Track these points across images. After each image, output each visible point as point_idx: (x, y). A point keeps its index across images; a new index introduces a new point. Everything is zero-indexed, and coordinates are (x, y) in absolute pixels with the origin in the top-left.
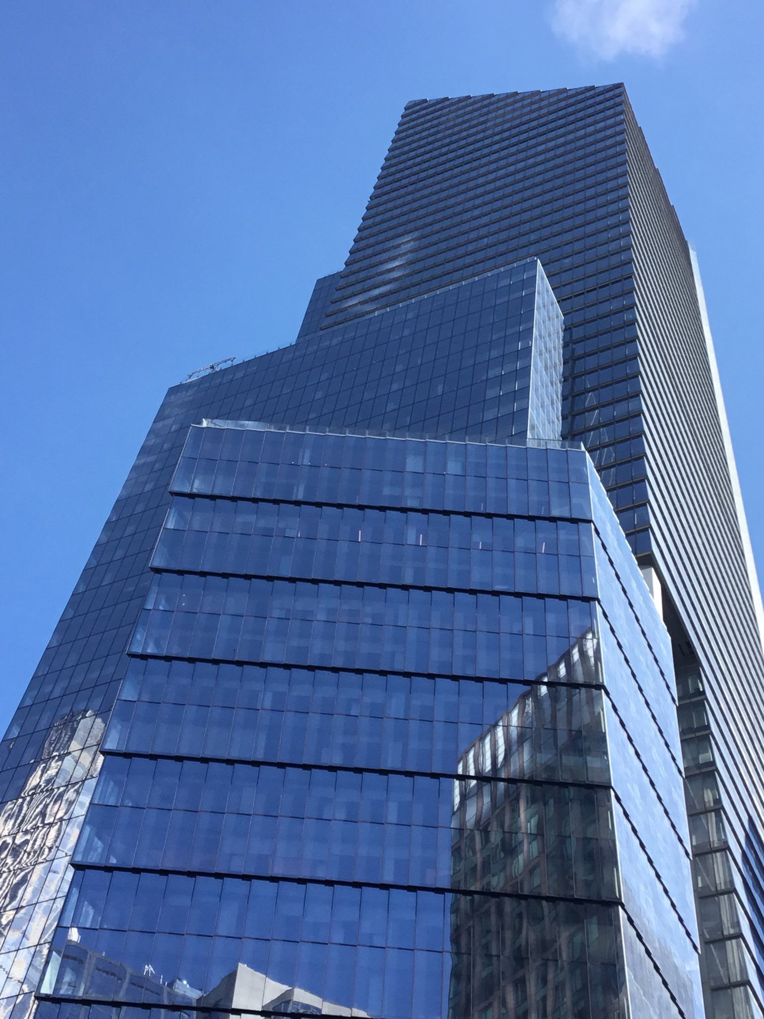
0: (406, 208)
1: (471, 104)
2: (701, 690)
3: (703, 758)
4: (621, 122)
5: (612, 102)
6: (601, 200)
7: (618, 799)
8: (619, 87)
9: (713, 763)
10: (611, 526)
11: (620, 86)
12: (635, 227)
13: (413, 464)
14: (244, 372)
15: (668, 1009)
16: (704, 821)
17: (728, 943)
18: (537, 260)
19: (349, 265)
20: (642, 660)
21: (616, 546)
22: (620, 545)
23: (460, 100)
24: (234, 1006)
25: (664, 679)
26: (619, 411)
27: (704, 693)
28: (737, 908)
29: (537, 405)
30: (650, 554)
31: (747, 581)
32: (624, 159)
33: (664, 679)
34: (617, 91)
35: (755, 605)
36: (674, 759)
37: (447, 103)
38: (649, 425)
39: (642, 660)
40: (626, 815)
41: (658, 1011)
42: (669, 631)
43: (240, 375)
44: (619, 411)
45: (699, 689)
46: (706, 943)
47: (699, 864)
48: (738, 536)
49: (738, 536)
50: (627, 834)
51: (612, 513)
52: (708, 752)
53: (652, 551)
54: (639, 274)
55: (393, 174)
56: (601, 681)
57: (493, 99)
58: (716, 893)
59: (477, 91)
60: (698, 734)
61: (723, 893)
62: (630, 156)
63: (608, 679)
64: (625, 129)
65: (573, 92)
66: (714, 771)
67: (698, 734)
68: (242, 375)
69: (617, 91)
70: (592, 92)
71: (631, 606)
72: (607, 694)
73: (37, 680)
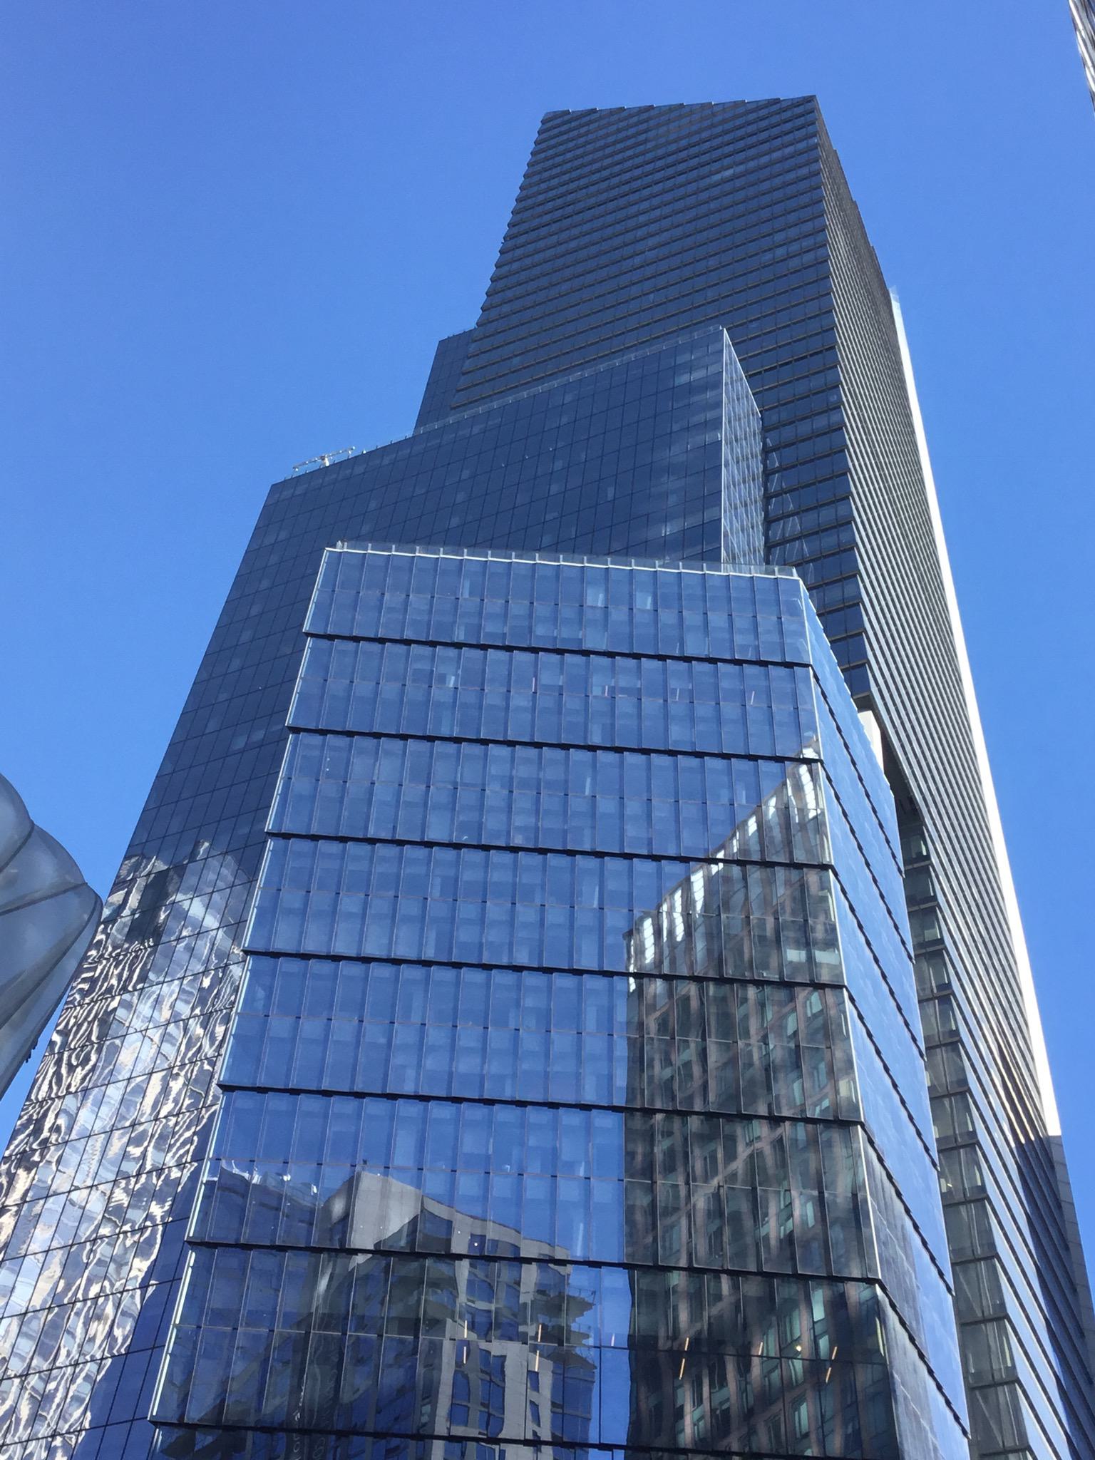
0: (566, 177)
1: (626, 119)
2: (925, 853)
3: (929, 935)
4: (815, 147)
5: (803, 132)
6: (790, 190)
7: (852, 999)
8: (810, 101)
9: (941, 941)
10: (830, 667)
11: (811, 99)
12: (837, 301)
13: (595, 598)
14: (365, 466)
15: (857, 785)
16: (984, 1327)
17: (1000, 1389)
18: (723, 330)
19: (491, 295)
20: (867, 826)
21: (836, 692)
22: (840, 690)
23: (612, 112)
24: (436, 1433)
25: (890, 847)
26: (827, 515)
27: (935, 898)
28: (992, 1224)
29: (737, 529)
30: (868, 696)
31: (1008, 938)
32: (817, 168)
33: (890, 847)
34: (809, 106)
35: (1001, 876)
36: (903, 943)
37: (594, 116)
38: (861, 535)
39: (867, 826)
40: (861, 1017)
41: (902, 1244)
42: (892, 788)
43: (359, 469)
44: (827, 515)
45: (921, 852)
46: (959, 1264)
47: (969, 1295)
48: (977, 781)
49: (977, 781)
50: (863, 1039)
51: (828, 651)
52: (934, 927)
53: (871, 692)
54: (842, 343)
55: (534, 195)
56: (833, 919)
57: (652, 113)
58: (982, 1319)
59: (630, 102)
60: (923, 906)
61: (1002, 1384)
62: (827, 193)
63: (822, 725)
64: (821, 169)
65: (754, 106)
66: (949, 995)
67: (923, 906)
68: (363, 471)
69: (809, 106)
70: (778, 106)
71: (854, 763)
72: (836, 875)
73: (259, 531)
